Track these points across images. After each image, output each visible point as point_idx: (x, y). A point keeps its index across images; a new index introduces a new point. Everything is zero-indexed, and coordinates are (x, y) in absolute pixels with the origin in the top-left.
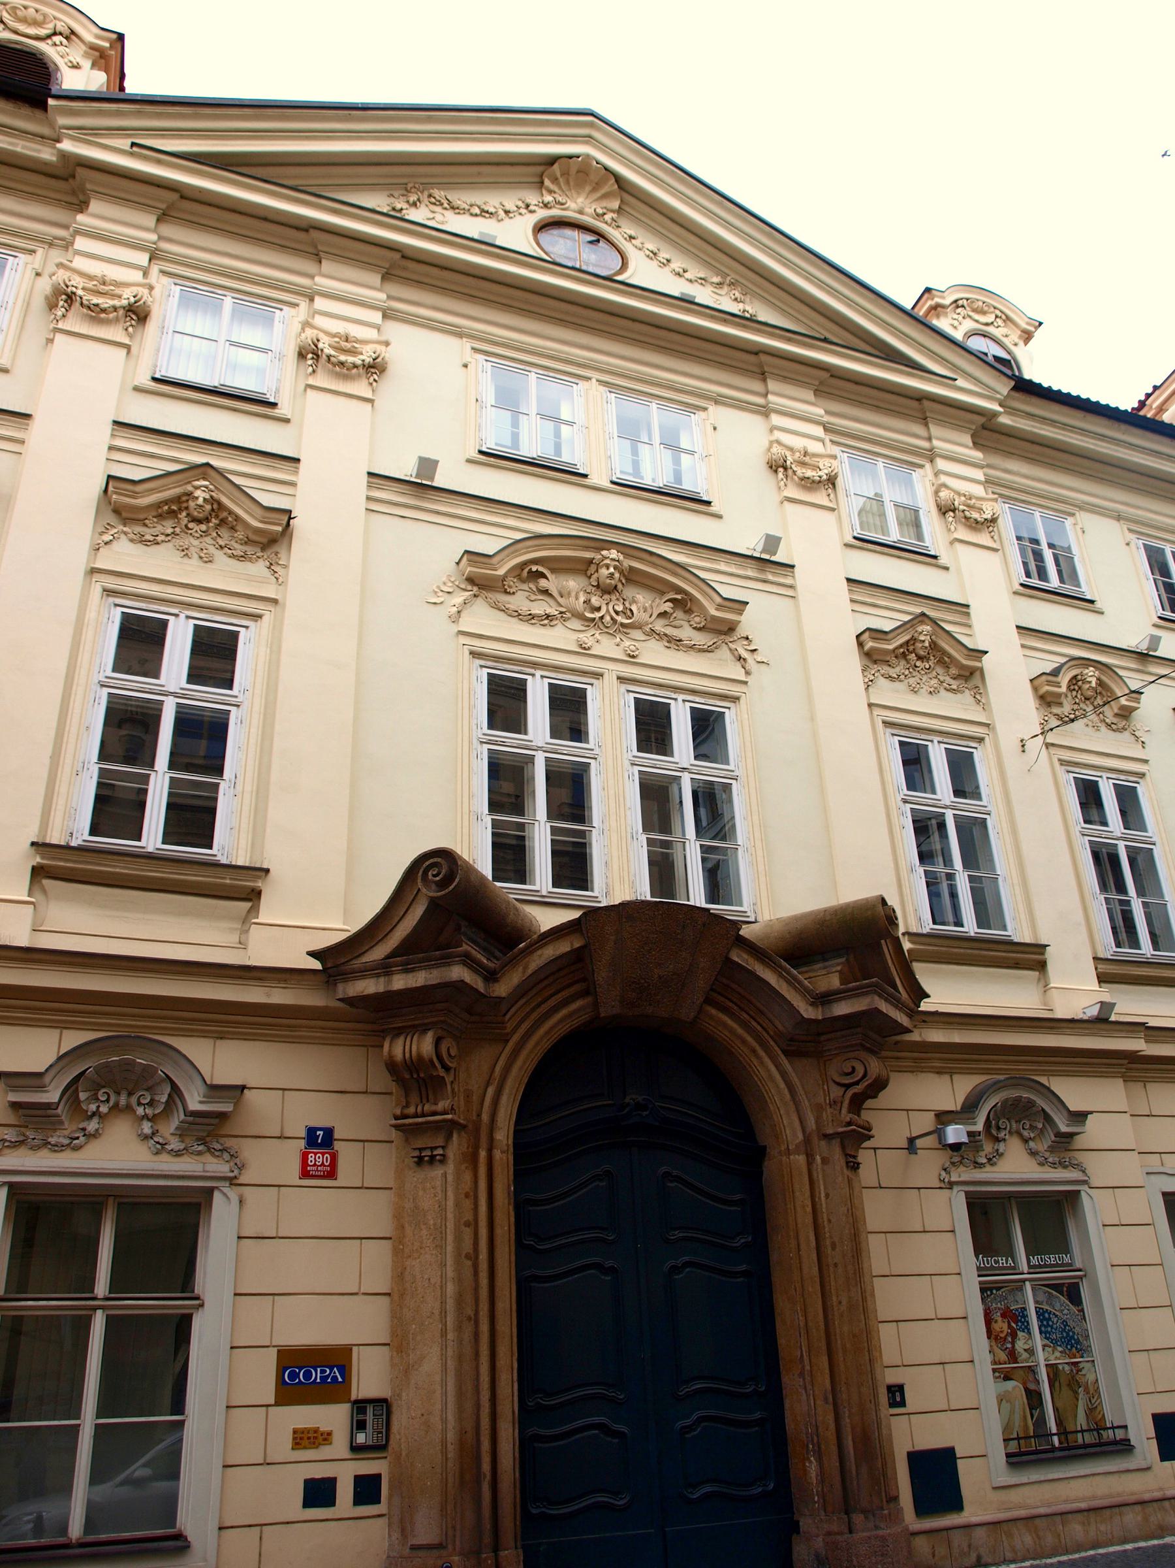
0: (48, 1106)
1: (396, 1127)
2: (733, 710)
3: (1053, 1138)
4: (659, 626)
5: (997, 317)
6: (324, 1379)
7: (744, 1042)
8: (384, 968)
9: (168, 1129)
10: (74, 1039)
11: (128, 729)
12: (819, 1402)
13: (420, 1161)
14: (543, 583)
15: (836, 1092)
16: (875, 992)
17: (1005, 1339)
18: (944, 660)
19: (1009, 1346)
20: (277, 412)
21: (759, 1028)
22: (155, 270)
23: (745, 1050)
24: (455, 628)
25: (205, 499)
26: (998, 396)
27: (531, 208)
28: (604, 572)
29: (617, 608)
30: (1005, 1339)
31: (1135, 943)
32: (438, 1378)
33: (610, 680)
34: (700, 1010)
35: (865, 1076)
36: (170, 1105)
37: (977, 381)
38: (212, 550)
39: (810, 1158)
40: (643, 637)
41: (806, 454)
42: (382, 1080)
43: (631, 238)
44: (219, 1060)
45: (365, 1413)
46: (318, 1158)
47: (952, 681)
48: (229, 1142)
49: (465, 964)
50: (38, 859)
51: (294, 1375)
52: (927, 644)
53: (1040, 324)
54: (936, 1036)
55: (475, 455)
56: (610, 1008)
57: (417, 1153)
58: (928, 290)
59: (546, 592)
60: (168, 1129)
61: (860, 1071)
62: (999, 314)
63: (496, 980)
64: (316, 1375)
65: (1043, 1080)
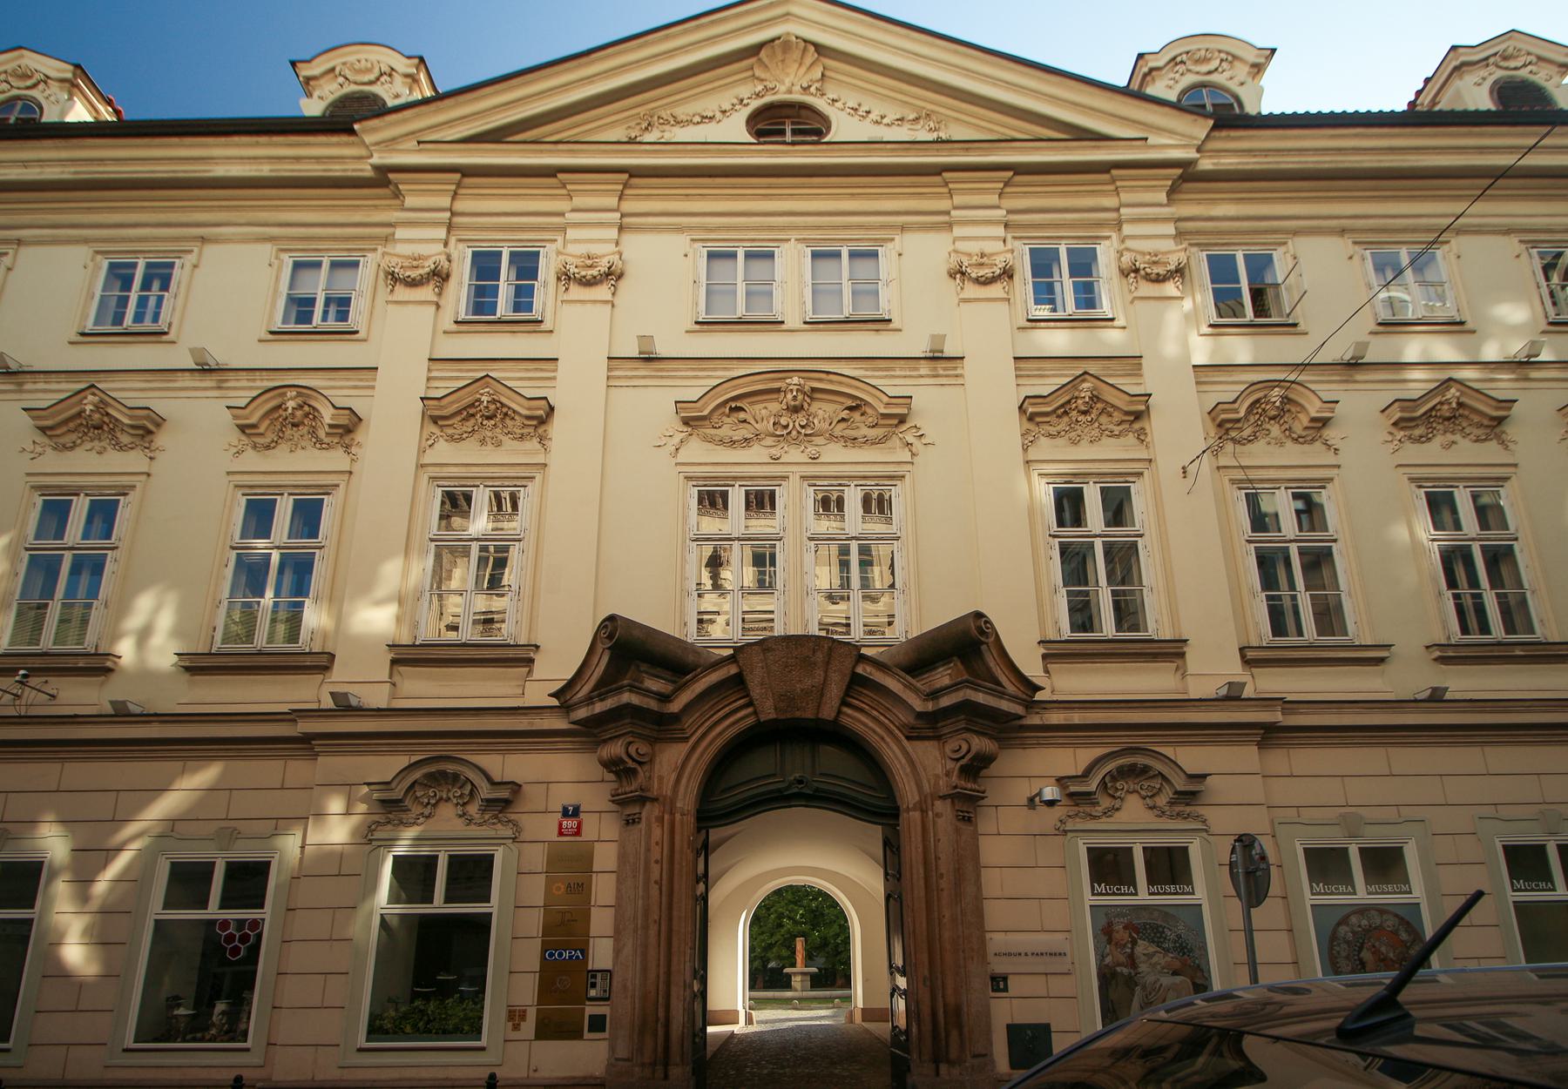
0: (1089, 794)
2: (529, 489)
4: (839, 430)
8: (589, 700)
9: (473, 809)
10: (403, 761)
11: (42, 568)
13: (628, 823)
14: (742, 415)
15: (950, 765)
20: (1465, 327)
22: (453, 240)
24: (674, 461)
28: (789, 396)
31: (1485, 628)
33: (794, 480)
34: (839, 712)
36: (471, 793)
37: (1171, 132)
39: (924, 812)
41: (983, 255)
42: (598, 771)
44: (1192, 758)
46: (569, 824)
48: (1202, 811)
50: (1044, 651)
51: (551, 955)
53: (1273, 51)
54: (1055, 718)
55: (1545, 327)
56: (768, 712)
58: (1140, 56)
60: (473, 809)
61: (965, 747)
62: (1223, 56)
65: (1168, 751)
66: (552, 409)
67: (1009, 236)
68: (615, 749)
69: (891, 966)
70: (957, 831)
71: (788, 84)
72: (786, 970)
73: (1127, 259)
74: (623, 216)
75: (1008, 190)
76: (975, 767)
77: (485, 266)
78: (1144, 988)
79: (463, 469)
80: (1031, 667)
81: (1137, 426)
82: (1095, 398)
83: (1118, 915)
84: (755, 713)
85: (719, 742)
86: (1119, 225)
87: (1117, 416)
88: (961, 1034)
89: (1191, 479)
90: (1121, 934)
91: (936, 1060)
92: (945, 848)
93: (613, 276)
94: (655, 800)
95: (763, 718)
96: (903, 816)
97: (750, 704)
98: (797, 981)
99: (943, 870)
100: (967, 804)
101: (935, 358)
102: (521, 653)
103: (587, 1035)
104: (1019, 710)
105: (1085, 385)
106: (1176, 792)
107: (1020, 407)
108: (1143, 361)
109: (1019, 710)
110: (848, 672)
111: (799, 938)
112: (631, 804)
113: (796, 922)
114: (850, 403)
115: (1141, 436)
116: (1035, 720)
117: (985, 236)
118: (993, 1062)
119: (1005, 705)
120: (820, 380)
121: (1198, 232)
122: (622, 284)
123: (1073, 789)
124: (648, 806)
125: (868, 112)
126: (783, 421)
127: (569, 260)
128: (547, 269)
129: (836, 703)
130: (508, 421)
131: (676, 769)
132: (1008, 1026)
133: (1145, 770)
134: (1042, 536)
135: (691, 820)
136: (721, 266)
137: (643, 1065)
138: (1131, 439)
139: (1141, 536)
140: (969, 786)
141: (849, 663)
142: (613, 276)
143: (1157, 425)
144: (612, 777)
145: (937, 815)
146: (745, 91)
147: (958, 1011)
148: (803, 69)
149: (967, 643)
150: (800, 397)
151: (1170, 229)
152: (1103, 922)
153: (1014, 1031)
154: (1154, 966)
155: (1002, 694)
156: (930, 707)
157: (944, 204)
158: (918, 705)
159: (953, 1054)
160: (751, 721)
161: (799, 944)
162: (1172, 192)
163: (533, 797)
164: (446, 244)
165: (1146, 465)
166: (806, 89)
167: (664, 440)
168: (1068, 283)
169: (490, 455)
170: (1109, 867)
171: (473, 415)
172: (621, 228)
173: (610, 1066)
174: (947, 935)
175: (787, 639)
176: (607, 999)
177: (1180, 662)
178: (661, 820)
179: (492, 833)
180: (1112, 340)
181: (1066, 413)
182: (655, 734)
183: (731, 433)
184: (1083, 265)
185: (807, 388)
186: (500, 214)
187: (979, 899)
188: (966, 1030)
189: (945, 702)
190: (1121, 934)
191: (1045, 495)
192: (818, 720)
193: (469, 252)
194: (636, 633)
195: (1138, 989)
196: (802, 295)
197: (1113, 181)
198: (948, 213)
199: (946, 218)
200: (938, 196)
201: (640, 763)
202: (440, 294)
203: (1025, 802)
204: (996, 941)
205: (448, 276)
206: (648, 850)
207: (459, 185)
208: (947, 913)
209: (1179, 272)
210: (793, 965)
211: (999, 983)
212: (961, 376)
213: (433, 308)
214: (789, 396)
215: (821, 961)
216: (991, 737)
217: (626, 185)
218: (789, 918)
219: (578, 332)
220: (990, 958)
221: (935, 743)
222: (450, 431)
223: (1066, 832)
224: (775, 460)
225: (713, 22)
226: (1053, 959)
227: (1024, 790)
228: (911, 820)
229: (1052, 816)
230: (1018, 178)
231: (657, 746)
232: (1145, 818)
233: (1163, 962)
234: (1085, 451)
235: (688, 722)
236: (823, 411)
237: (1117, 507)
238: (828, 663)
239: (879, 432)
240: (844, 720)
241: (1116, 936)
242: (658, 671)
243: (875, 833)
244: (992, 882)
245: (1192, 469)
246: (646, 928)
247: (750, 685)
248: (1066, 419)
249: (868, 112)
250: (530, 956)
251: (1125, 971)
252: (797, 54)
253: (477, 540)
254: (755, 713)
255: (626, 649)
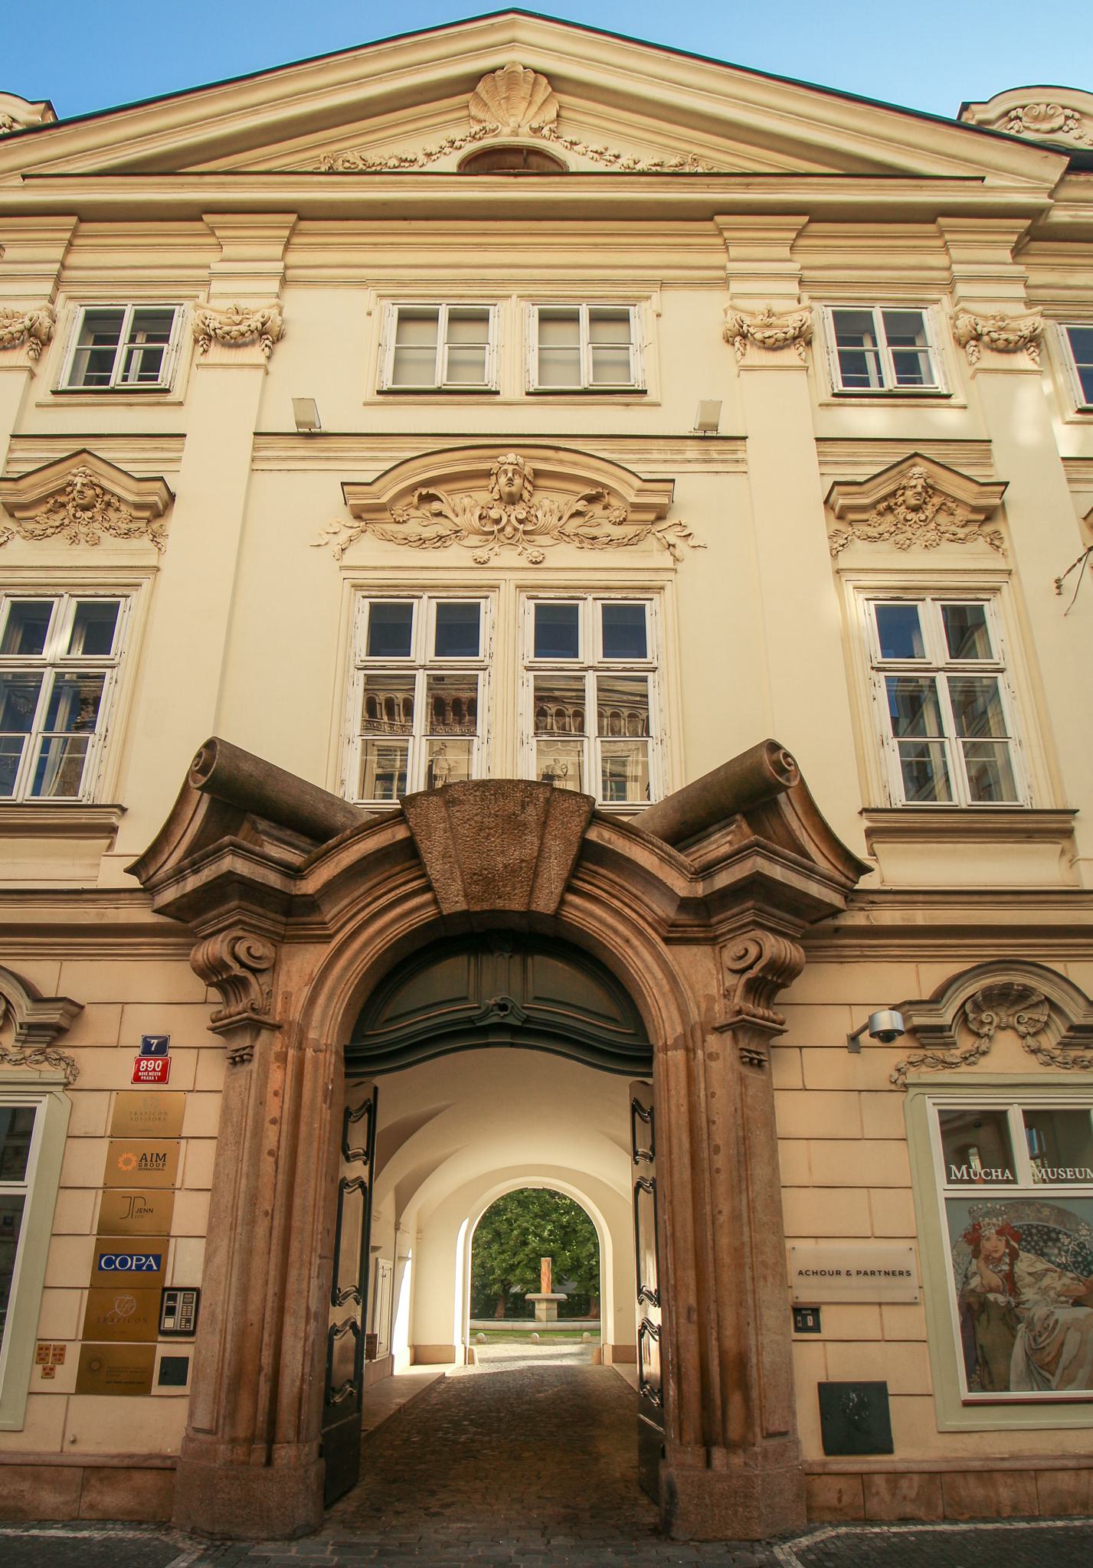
0: (941, 1029)
1: (213, 1029)
3: (1064, 1033)
4: (572, 526)
5: (1067, 118)
6: (139, 1267)
7: (616, 931)
8: (179, 875)
12: (682, 1321)
14: (436, 506)
15: (731, 980)
16: (758, 854)
17: (1000, 1259)
18: (949, 504)
19: (1006, 1268)
21: (634, 916)
22: (61, 298)
23: (618, 940)
25: (83, 485)
26: (1047, 185)
27: (457, 144)
28: (503, 480)
29: (520, 517)
30: (1000, 1259)
32: (224, 1270)
33: (508, 591)
34: (562, 902)
35: (759, 957)
38: (99, 533)
39: (690, 1051)
40: (551, 542)
41: (770, 314)
42: (196, 987)
43: (573, 144)
45: (175, 1300)
46: (153, 1064)
47: (959, 530)
49: (234, 854)
52: (919, 489)
54: (888, 916)
56: (455, 901)
57: (230, 1054)
59: (439, 514)
61: (753, 951)
62: (1069, 112)
63: (303, 878)
64: (132, 1263)
66: (172, 497)
67: (805, 296)
68: (215, 948)
69: (640, 1291)
70: (742, 1080)
71: (513, 123)
72: (529, 1296)
73: (964, 323)
74: (286, 267)
75: (802, 242)
76: (770, 982)
77: (100, 326)
78: (1030, 1325)
79: (42, 574)
80: (854, 839)
81: (988, 528)
82: (930, 489)
83: (989, 1213)
84: (435, 901)
85: (380, 944)
86: (950, 285)
87: (962, 514)
88: (747, 1399)
89: (1067, 596)
90: (994, 1243)
91: (707, 1442)
92: (722, 1109)
93: (269, 335)
94: (276, 1027)
95: (447, 908)
96: (659, 1057)
97: (428, 888)
98: (541, 1309)
99: (719, 1139)
100: (757, 1037)
101: (707, 436)
102: (98, 818)
103: (156, 1389)
104: (835, 899)
105: (916, 470)
106: (1072, 1028)
107: (826, 502)
108: (993, 446)
109: (835, 899)
110: (575, 839)
111: (530, 1256)
112: (241, 1030)
113: (543, 1240)
114: (588, 491)
115: (995, 542)
116: (858, 919)
117: (772, 280)
118: (797, 1442)
119: (814, 889)
120: (546, 459)
121: (1053, 302)
122: (281, 347)
123: (918, 1021)
124: (265, 1035)
125: (617, 157)
126: (494, 514)
127: (208, 313)
128: (181, 331)
129: (557, 887)
130: (111, 514)
131: (313, 986)
132: (822, 1387)
133: (1025, 993)
134: (862, 671)
135: (331, 1061)
136: (417, 332)
137: (233, 1441)
138: (981, 544)
139: (1001, 671)
140: (760, 1011)
141: (576, 824)
142: (269, 335)
143: (1016, 526)
144: (214, 994)
145: (712, 1057)
146: (457, 133)
147: (742, 1361)
148: (534, 108)
149: (756, 791)
150: (518, 481)
151: (1019, 291)
152: (967, 1223)
153: (829, 1392)
154: (1045, 1291)
155: (810, 872)
156: (700, 890)
157: (719, 258)
158: (681, 886)
159: (735, 1430)
160: (430, 912)
161: (545, 1264)
162: (1018, 252)
163: (99, 1024)
164: (52, 301)
165: (1005, 577)
166: (537, 131)
167: (327, 538)
168: (886, 353)
169: (84, 556)
170: (973, 1136)
171: (63, 505)
172: (284, 281)
173: (188, 1439)
174: (724, 1241)
175: (483, 784)
176: (192, 1333)
177: (1065, 843)
178: (282, 1058)
179: (34, 1076)
180: (945, 421)
181: (890, 509)
182: (280, 929)
183: (420, 530)
184: (906, 330)
185: (527, 471)
186: (125, 269)
187: (774, 1185)
188: (754, 1394)
189: (723, 880)
190: (994, 1243)
191: (863, 616)
192: (529, 914)
193: (81, 313)
194: (247, 767)
195: (1021, 1327)
196: (524, 361)
197: (941, 233)
198: (724, 268)
199: (721, 273)
200: (710, 248)
201: (255, 971)
202: (37, 360)
203: (844, 1042)
204: (802, 1253)
205: (49, 339)
206: (261, 1102)
207: (75, 233)
208: (725, 1207)
209: (1033, 341)
210: (538, 1290)
211: (806, 1317)
212: (743, 461)
213: (25, 375)
214: (503, 480)
215: (572, 1286)
216: (792, 939)
217: (294, 231)
218: (536, 1235)
219: (213, 404)
220: (793, 1278)
221: (708, 949)
222: (30, 526)
223: (906, 1086)
224: (482, 564)
225: (415, 44)
226: (891, 1279)
227: (841, 1025)
228: (671, 1062)
229: (884, 1061)
230: (815, 227)
231: (285, 949)
232: (1029, 1068)
233: (1058, 1285)
234: (917, 558)
235: (330, 912)
236: (550, 504)
237: (965, 628)
238: (544, 825)
239: (628, 530)
240: (571, 915)
241: (987, 1246)
242: (286, 834)
243: (619, 1088)
244: (796, 1162)
245: (1069, 582)
246: (252, 1223)
247: (427, 857)
248: (890, 518)
249: (617, 157)
250: (77, 1263)
251: (1001, 1299)
252: (525, 89)
253: (53, 665)
254: (435, 901)
255: (234, 793)
